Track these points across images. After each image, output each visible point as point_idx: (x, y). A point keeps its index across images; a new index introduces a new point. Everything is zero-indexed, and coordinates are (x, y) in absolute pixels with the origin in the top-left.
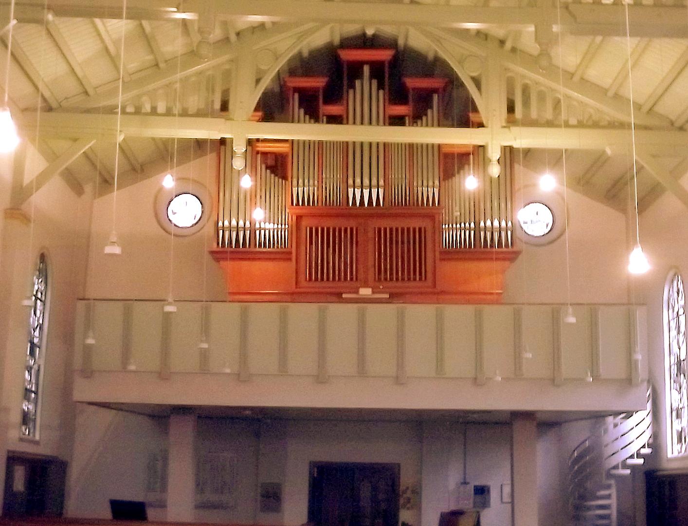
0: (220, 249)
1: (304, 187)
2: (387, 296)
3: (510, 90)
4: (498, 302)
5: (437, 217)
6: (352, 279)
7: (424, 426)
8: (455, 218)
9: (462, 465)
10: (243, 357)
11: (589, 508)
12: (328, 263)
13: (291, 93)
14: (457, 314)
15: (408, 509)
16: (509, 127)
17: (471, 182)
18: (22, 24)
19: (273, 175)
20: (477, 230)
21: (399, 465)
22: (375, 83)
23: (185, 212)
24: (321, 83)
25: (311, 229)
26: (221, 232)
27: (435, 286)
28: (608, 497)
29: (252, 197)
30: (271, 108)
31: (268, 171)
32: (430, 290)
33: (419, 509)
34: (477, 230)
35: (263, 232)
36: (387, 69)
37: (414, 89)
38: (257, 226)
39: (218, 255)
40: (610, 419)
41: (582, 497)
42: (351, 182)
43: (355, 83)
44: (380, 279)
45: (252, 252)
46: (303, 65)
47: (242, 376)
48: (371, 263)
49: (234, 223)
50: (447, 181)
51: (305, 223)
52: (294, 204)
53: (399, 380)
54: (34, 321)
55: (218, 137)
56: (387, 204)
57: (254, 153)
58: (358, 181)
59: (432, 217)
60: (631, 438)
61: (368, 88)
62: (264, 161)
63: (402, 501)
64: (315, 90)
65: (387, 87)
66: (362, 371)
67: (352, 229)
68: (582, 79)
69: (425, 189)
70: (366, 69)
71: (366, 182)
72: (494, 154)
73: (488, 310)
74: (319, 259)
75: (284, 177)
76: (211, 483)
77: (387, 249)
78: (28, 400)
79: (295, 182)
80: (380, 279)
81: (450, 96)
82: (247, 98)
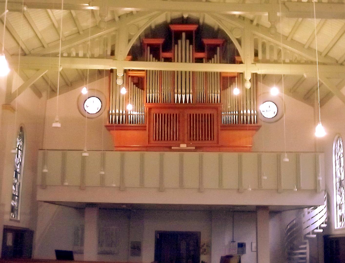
0: (110, 124)
1: (152, 93)
2: (194, 148)
3: (256, 45)
4: (250, 151)
5: (219, 108)
6: (176, 140)
7: (213, 213)
8: (228, 109)
9: (232, 233)
10: (122, 179)
11: (295, 254)
12: (164, 132)
13: (146, 46)
14: (229, 157)
15: (205, 254)
16: (255, 64)
17: (236, 91)
18: (11, 12)
19: (137, 88)
20: (239, 115)
21: (200, 232)
22: (188, 41)
23: (93, 106)
24: (161, 41)
25: (156, 115)
26: (111, 116)
27: (218, 143)
28: (305, 248)
29: (127, 99)
30: (136, 54)
31: (135, 86)
32: (216, 145)
33: (210, 254)
34: (239, 115)
35: (132, 116)
36: (194, 35)
37: (207, 45)
38: (129, 113)
39: (109, 128)
40: (306, 210)
41: (292, 249)
42: (176, 91)
43: (178, 42)
44: (190, 140)
45: (126, 126)
46: (152, 33)
47: (121, 188)
48: (186, 131)
49: (117, 111)
50: (224, 90)
51: (153, 111)
52: (148, 102)
53: (200, 190)
54: (17, 161)
55: (109, 68)
56: (194, 102)
57: (128, 77)
58: (180, 90)
59: (217, 109)
60: (316, 219)
61: (185, 44)
62: (132, 81)
63: (201, 251)
64: (158, 45)
65: (194, 44)
66: (181, 186)
67: (176, 115)
68: (292, 39)
69: (213, 95)
70: (184, 35)
71: (184, 91)
72: (248, 77)
73: (245, 155)
74: (160, 129)
75: (143, 89)
76: (106, 242)
77: (194, 124)
78: (14, 200)
79: (148, 91)
80: (190, 140)
81: (226, 48)
82: (124, 49)
